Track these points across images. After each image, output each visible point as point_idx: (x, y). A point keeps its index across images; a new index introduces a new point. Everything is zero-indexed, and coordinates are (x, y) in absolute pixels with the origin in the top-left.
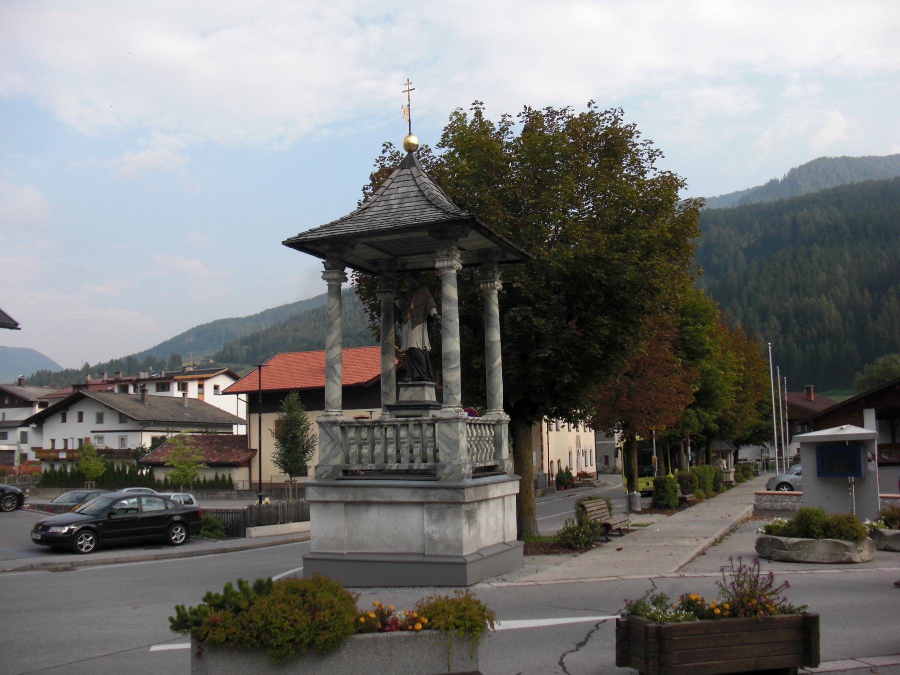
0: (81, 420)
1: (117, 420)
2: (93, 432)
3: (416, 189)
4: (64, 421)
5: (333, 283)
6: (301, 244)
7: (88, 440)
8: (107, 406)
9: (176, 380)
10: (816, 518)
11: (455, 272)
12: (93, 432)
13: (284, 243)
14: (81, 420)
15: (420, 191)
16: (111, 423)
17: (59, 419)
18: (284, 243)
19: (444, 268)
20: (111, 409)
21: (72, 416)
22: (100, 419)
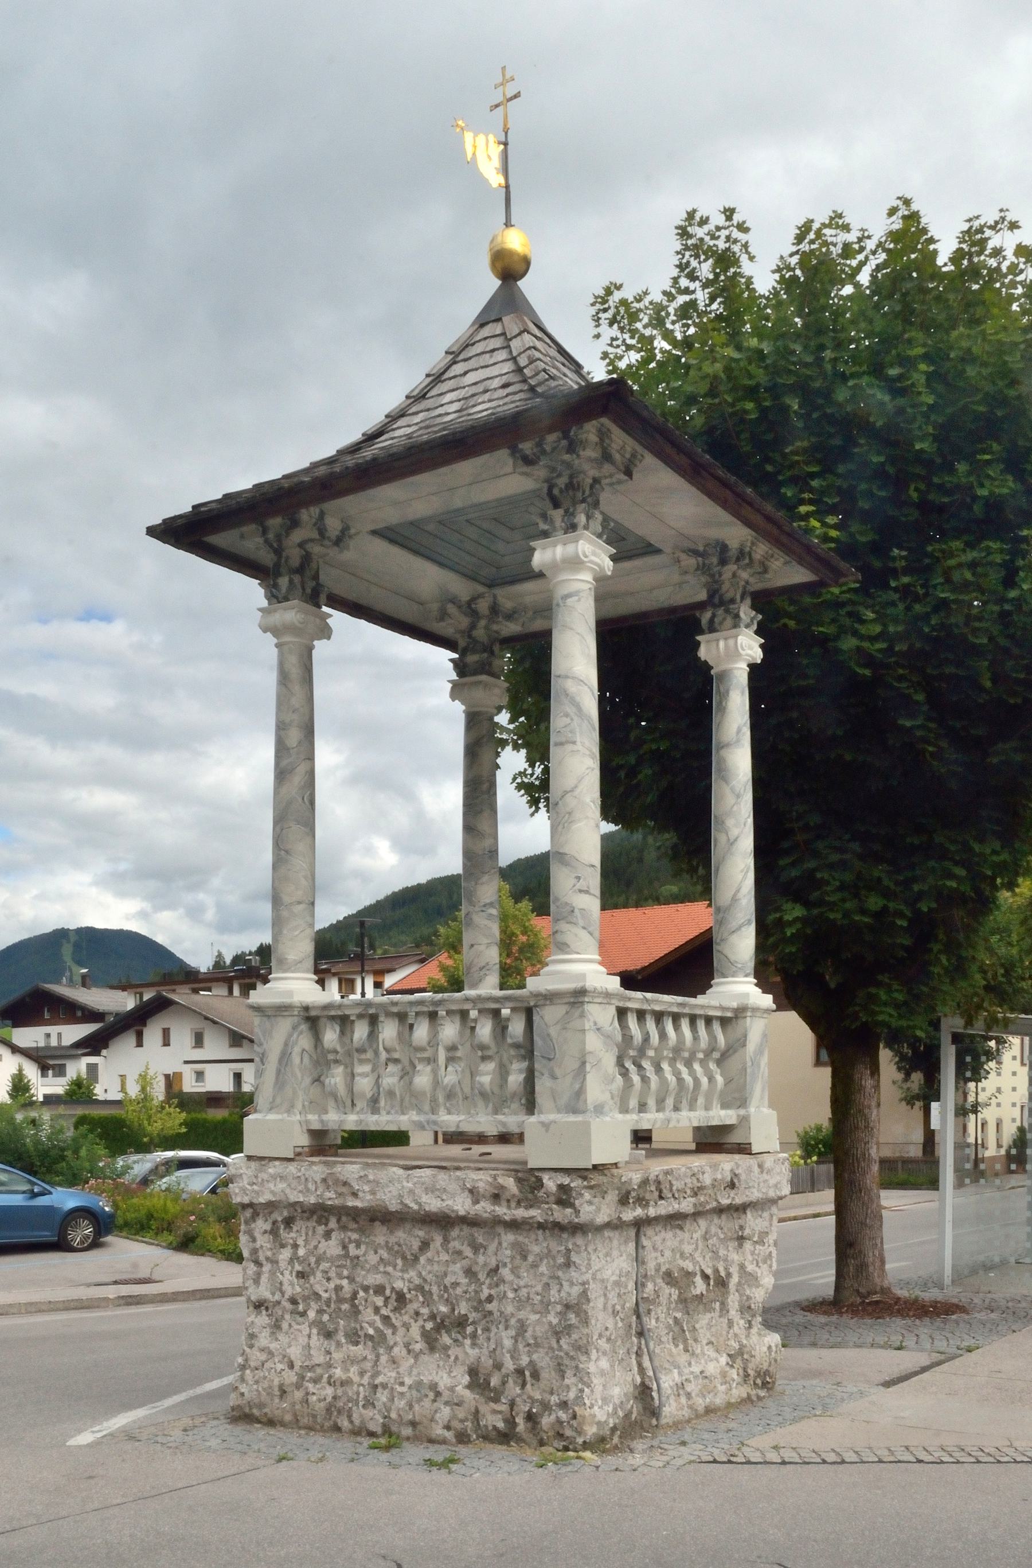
0: (166, 1043)
1: (225, 1041)
2: (186, 1062)
3: (508, 367)
4: (140, 1044)
5: (287, 638)
6: (194, 532)
7: (178, 1076)
8: (206, 1018)
9: (334, 974)
10: (874, 1104)
11: (588, 577)
12: (186, 1062)
13: (151, 531)
14: (166, 1043)
15: (519, 370)
16: (216, 1047)
17: (130, 1039)
18: (151, 531)
19: (556, 567)
20: (215, 1022)
21: (152, 1033)
22: (199, 1041)
